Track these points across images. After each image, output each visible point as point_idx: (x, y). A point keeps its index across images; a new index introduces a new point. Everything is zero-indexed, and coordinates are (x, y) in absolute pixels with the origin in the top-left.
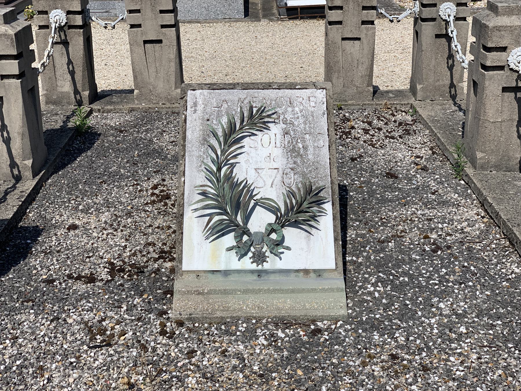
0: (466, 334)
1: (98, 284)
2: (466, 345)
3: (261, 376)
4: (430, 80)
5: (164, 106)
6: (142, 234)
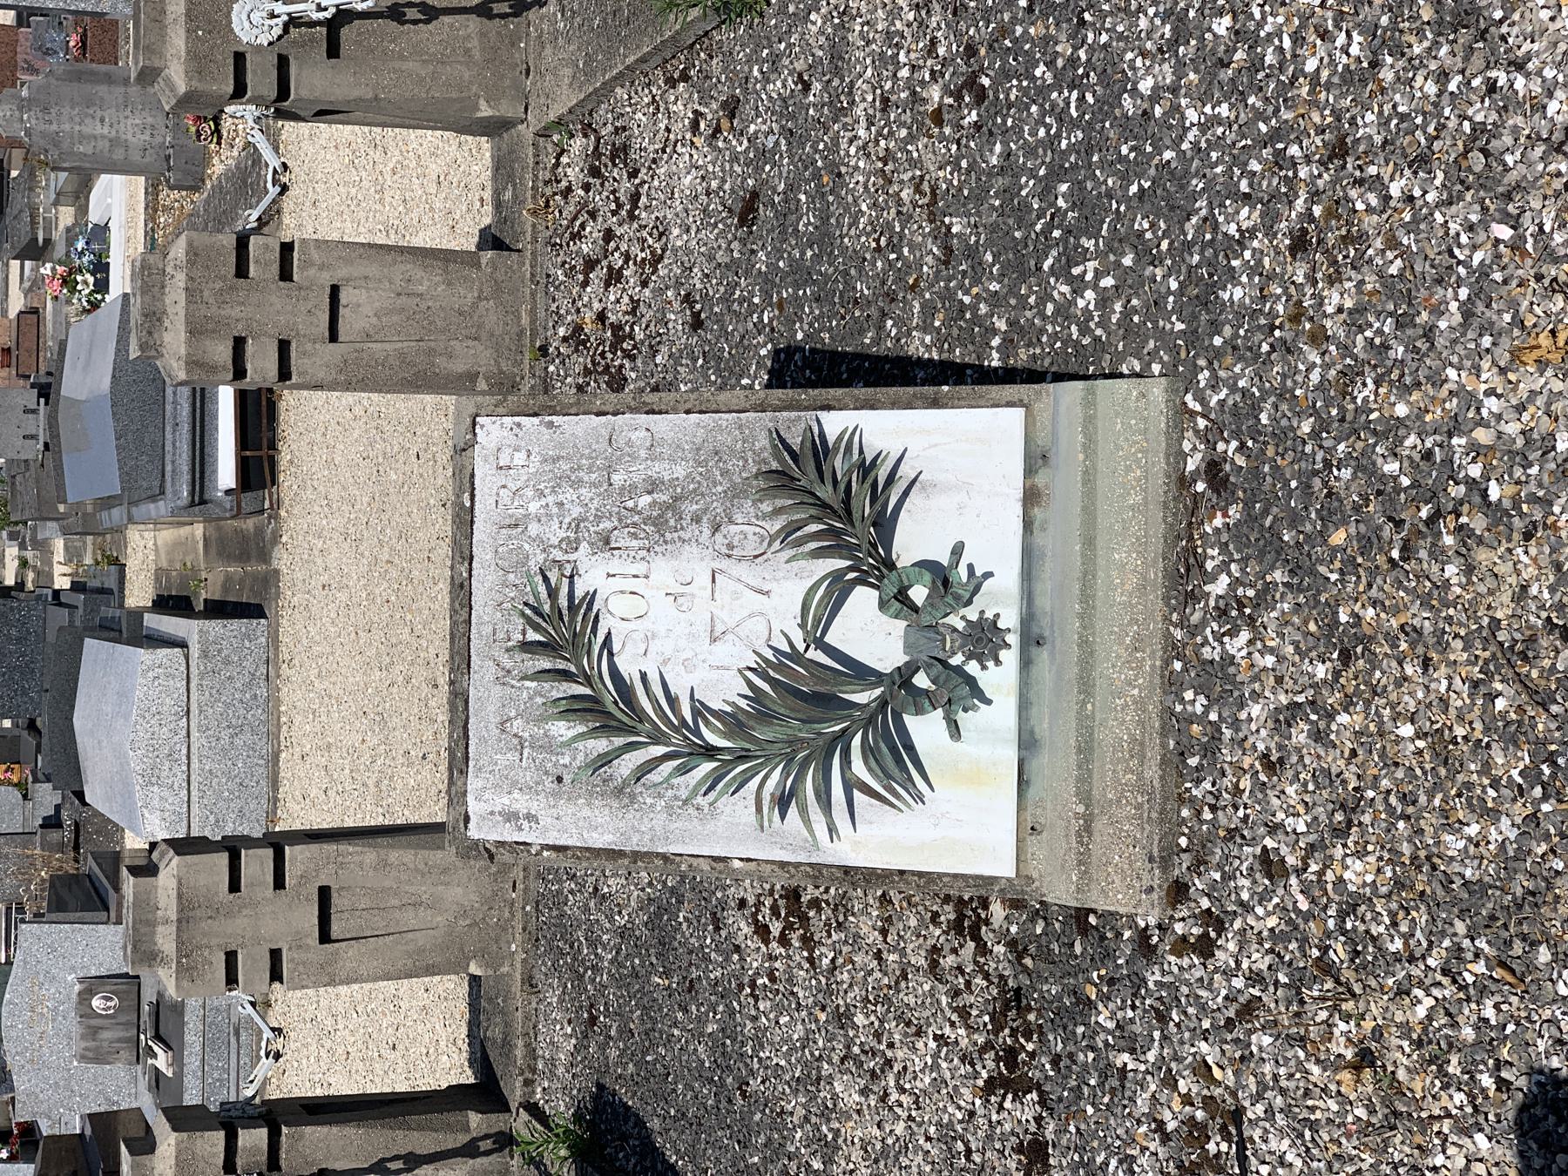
0: (1235, 18)
1: (1049, 1134)
2: (1270, 19)
3: (1346, 657)
4: (467, 75)
5: (520, 886)
6: (903, 984)
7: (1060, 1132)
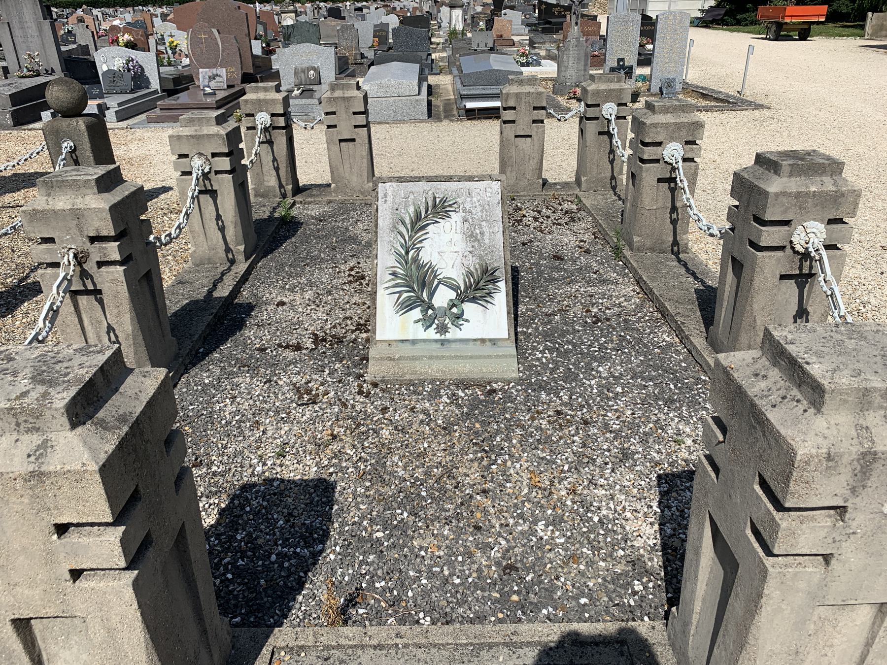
1: (303, 351)
3: (445, 428)
7: (304, 354)
